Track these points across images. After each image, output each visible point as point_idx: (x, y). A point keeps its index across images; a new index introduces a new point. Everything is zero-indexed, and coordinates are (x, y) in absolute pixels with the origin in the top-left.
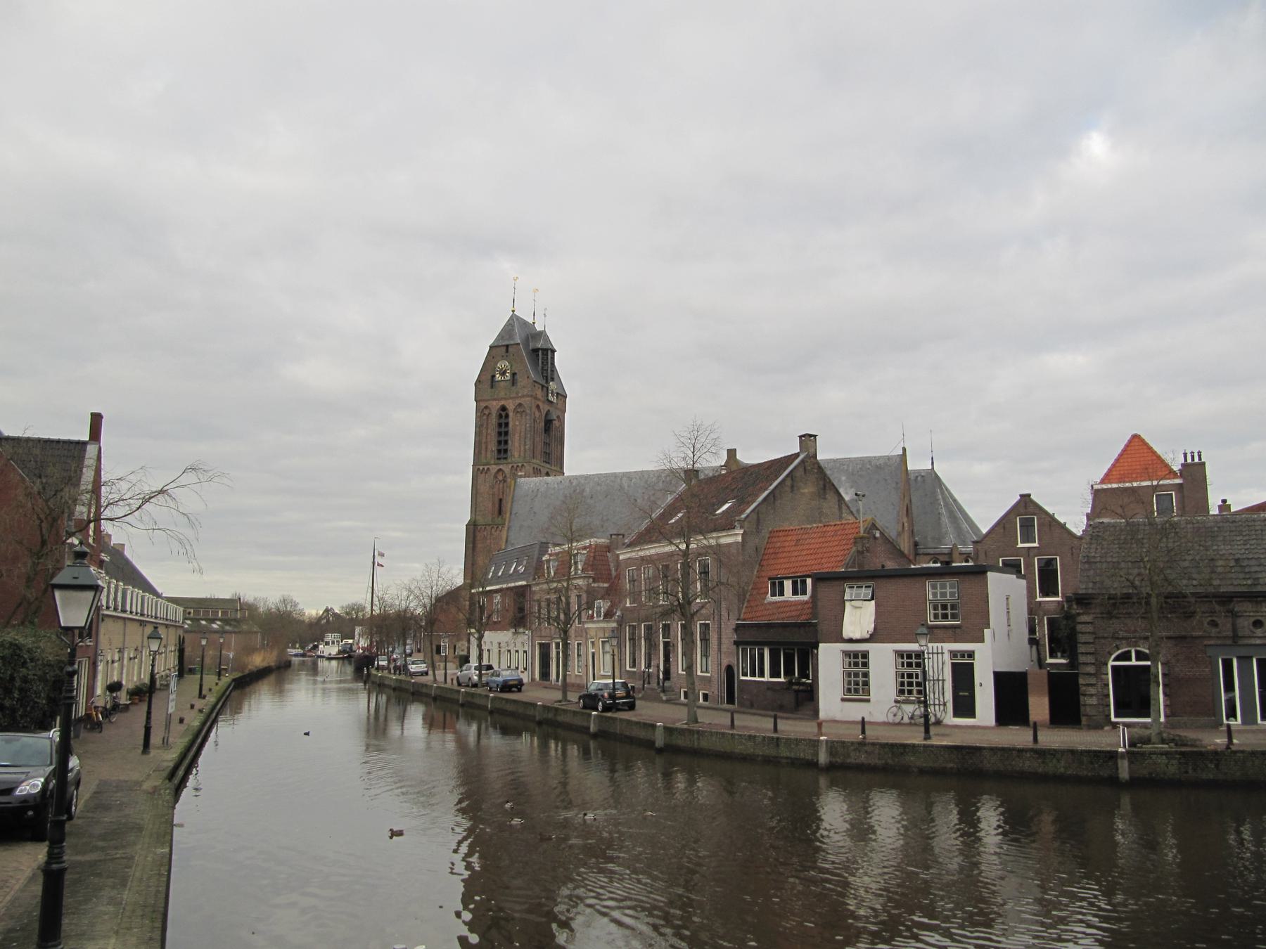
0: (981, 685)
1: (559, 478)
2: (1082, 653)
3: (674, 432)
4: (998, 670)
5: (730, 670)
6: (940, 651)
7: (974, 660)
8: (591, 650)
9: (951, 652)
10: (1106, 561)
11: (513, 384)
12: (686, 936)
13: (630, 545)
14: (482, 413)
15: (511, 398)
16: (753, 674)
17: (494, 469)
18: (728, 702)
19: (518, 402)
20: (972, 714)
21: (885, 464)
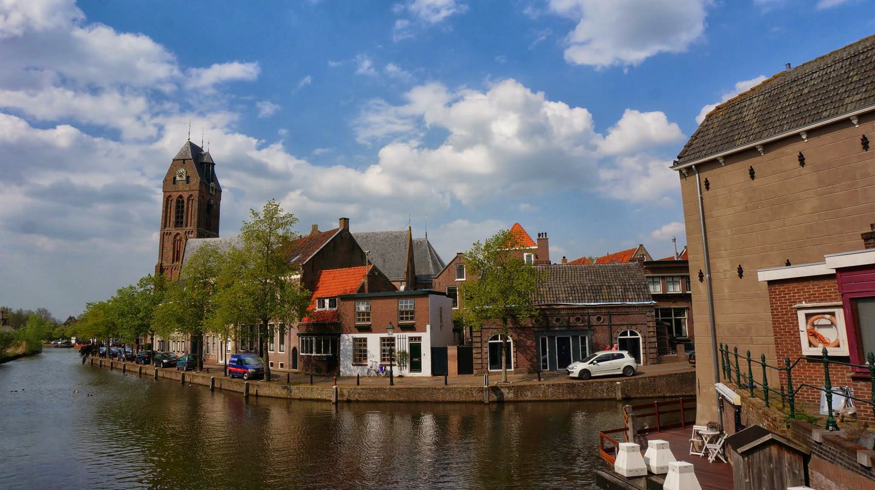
0: (424, 355)
2: (475, 337)
4: (435, 346)
6: (404, 337)
9: (409, 337)
11: (187, 183)
14: (167, 200)
18: (225, 376)
19: (190, 193)
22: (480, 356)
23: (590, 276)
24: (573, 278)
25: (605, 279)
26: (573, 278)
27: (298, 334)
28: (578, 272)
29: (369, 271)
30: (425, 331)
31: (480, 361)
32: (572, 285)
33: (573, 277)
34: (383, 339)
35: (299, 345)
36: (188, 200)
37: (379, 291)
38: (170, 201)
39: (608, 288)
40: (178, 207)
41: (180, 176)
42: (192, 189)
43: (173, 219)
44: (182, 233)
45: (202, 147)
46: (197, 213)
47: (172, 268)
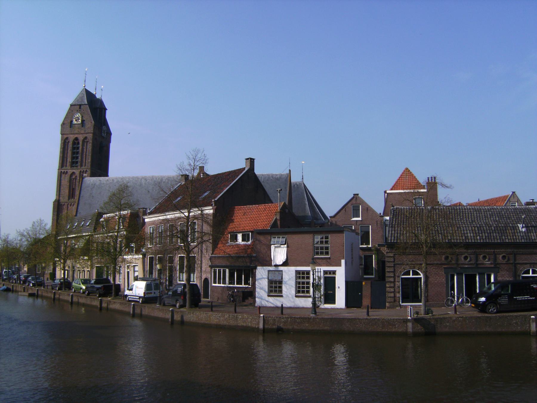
0: (339, 287)
1: (107, 178)
2: (388, 272)
3: (186, 153)
5: (206, 281)
6: (319, 271)
7: (336, 275)
8: (126, 270)
9: (324, 271)
10: (466, 222)
11: (82, 126)
13: (151, 213)
15: (81, 134)
16: (219, 283)
19: (85, 135)
20: (334, 302)
21: (280, 178)
22: (392, 290)
23: (494, 217)
24: (479, 219)
25: (509, 221)
26: (479, 219)
27: (210, 266)
28: (483, 213)
29: (280, 208)
30: (340, 265)
31: (392, 295)
32: (478, 226)
33: (478, 217)
34: (298, 272)
35: (211, 277)
36: (83, 141)
37: (289, 227)
38: (67, 143)
39: (512, 229)
40: (74, 148)
41: (76, 120)
42: (86, 132)
43: (69, 159)
44: (77, 172)
45: (95, 94)
46: (90, 154)
47: (68, 204)
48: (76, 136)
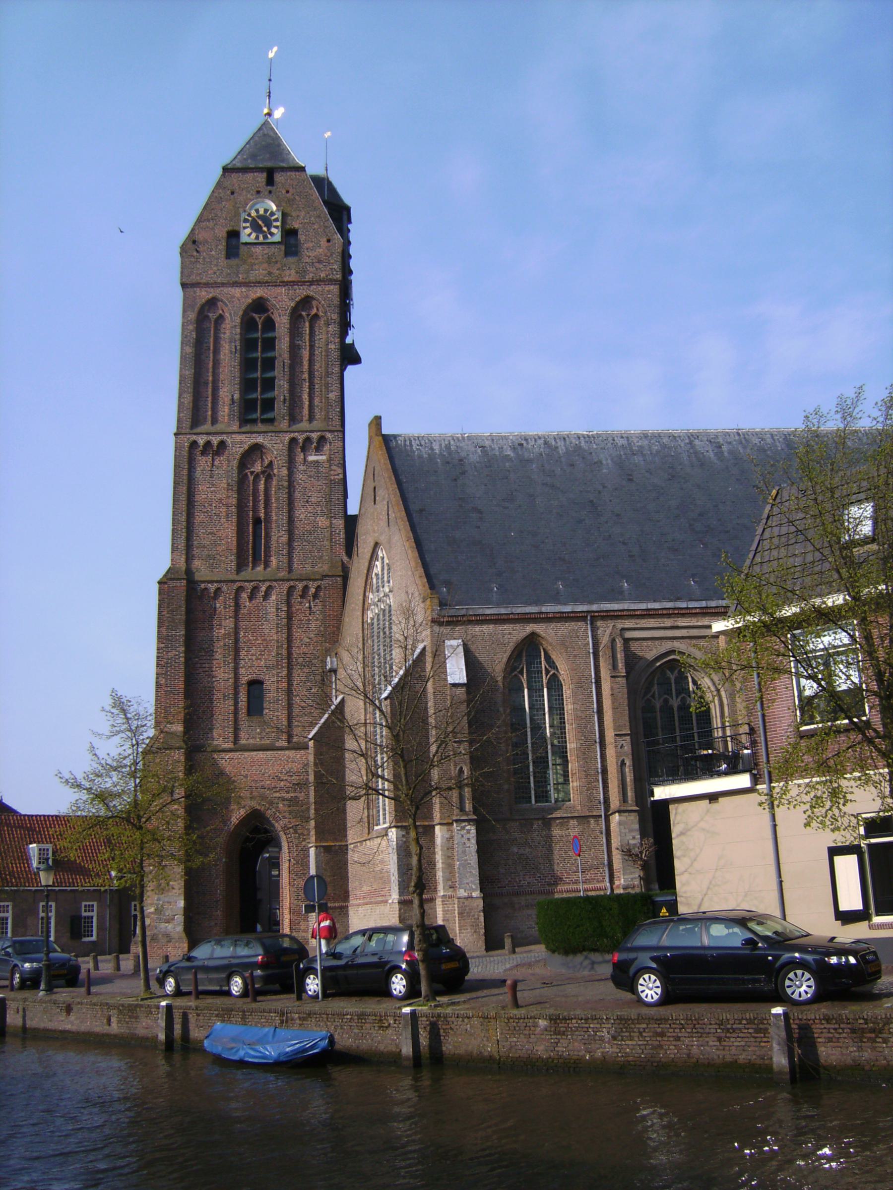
12: (839, 608)
15: (285, 284)
17: (239, 443)
36: (295, 316)
42: (309, 277)
48: (258, 295)
